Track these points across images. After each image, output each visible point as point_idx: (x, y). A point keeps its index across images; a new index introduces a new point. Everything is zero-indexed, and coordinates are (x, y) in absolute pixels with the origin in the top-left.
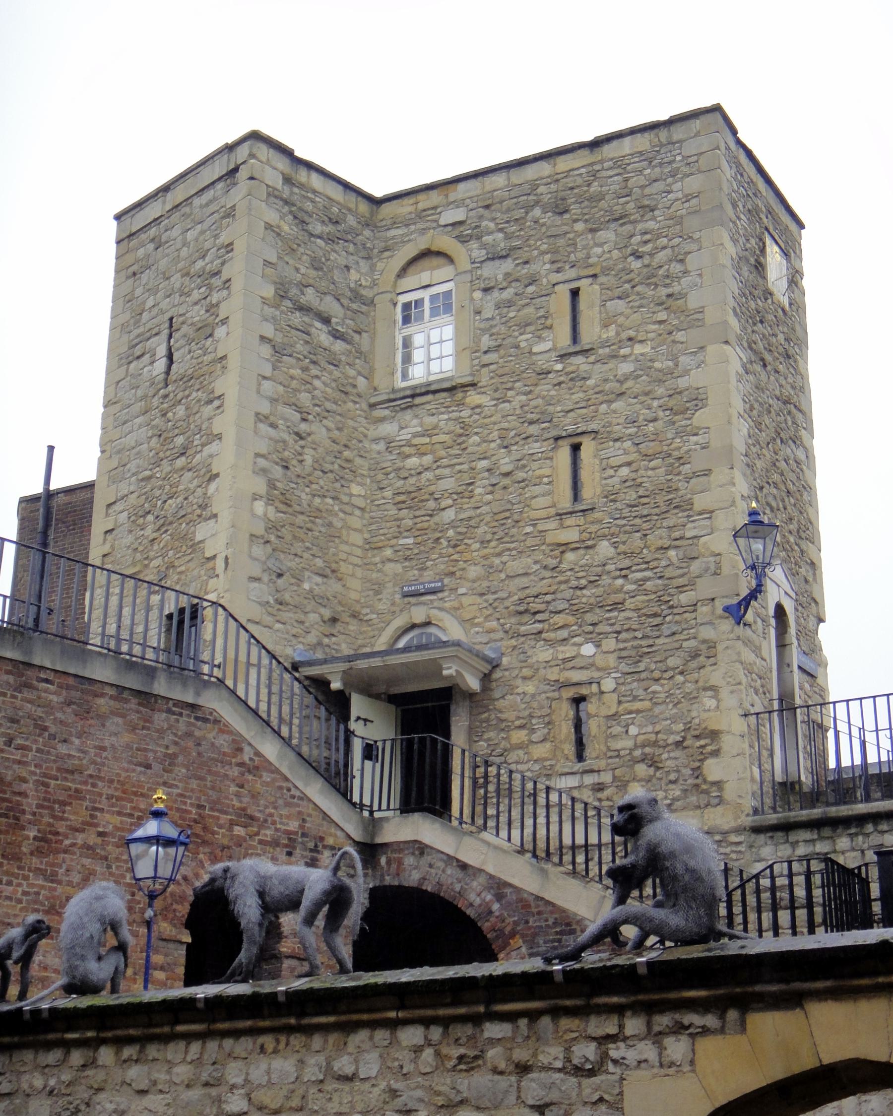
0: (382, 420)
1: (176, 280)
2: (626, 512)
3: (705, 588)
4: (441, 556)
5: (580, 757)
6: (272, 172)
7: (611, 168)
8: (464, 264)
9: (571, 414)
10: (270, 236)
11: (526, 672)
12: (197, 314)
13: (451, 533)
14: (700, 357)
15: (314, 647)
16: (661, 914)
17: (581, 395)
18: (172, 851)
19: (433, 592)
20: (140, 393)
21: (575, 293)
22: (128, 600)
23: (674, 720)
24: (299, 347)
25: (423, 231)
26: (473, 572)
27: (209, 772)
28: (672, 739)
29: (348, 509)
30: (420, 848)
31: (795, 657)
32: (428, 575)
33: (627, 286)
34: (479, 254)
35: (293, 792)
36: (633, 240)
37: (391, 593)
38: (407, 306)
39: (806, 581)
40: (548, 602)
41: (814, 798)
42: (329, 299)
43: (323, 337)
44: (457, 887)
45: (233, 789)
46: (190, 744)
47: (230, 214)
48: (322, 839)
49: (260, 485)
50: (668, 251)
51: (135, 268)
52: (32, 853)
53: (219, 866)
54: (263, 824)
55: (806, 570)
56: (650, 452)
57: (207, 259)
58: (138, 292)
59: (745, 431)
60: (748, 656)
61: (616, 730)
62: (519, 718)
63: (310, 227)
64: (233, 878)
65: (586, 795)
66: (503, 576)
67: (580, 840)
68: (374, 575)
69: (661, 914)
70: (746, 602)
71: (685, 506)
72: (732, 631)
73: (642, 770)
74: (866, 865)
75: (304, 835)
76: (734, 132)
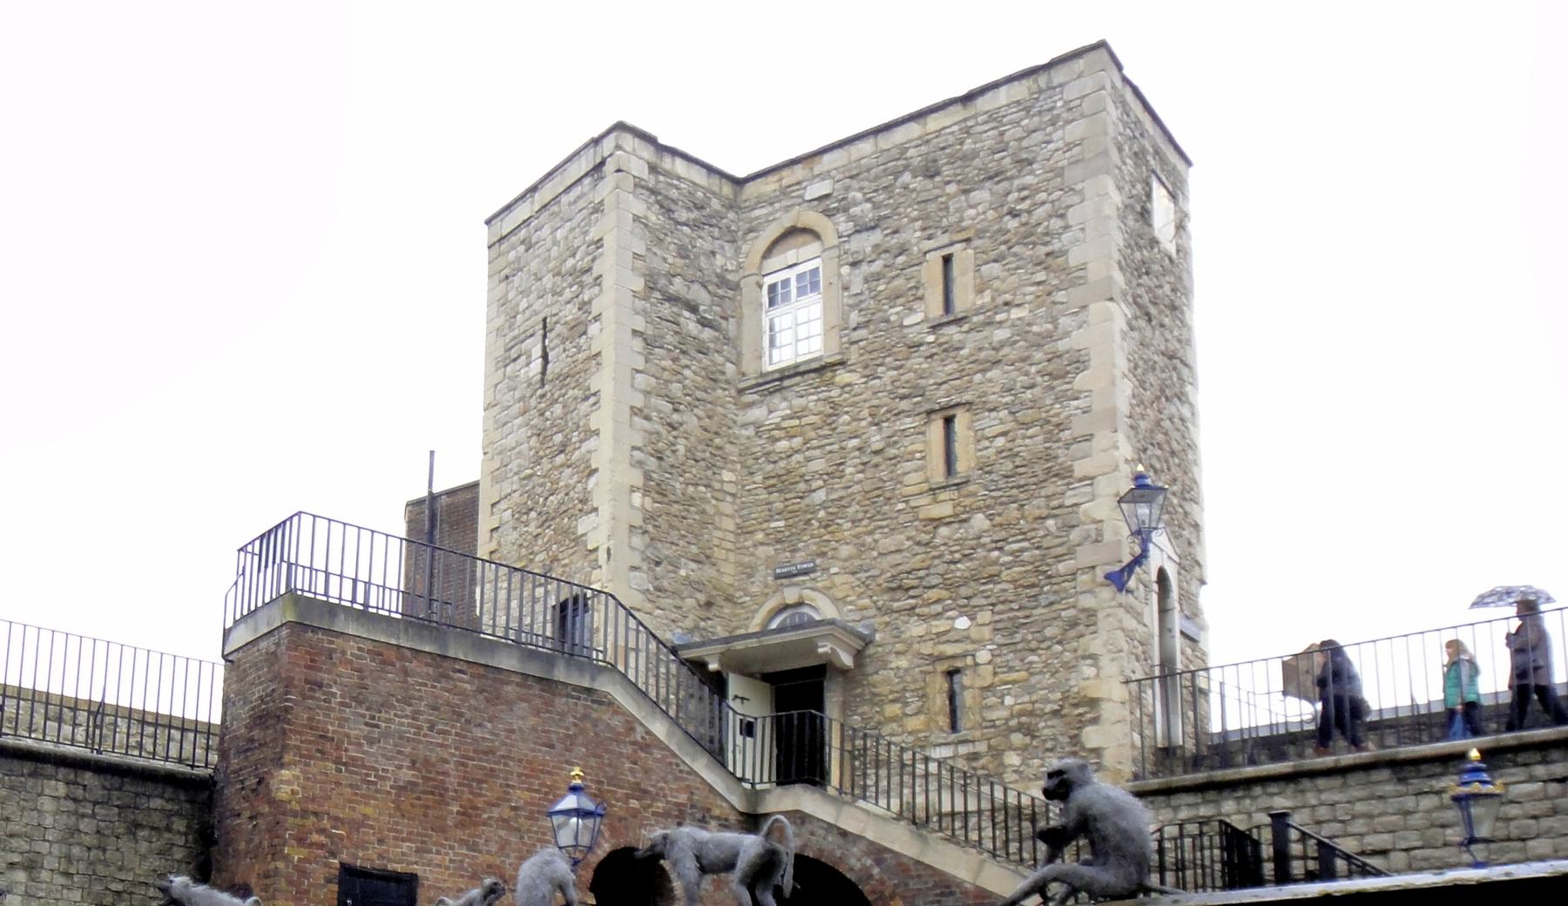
0: (751, 405)
1: (548, 281)
2: (1002, 484)
3: (1085, 556)
4: (813, 537)
5: (954, 727)
6: (637, 161)
7: (985, 122)
8: (831, 239)
9: (945, 386)
10: (639, 228)
11: (899, 647)
12: (570, 313)
13: (822, 514)
14: (1082, 316)
15: (691, 631)
16: (1089, 872)
17: (955, 366)
18: (590, 822)
19: (805, 573)
20: (517, 395)
21: (947, 260)
22: (515, 593)
23: (1051, 688)
24: (669, 338)
25: (787, 209)
26: (845, 551)
27: (607, 751)
28: (1048, 708)
29: (718, 495)
30: (800, 817)
31: (1177, 622)
32: (800, 556)
33: (1003, 247)
34: (846, 227)
35: (682, 767)
36: (1010, 198)
37: (763, 575)
38: (772, 288)
39: (1190, 544)
40: (921, 578)
41: (1196, 762)
42: (696, 287)
43: (692, 327)
44: (838, 853)
45: (628, 765)
46: (588, 725)
47: (598, 209)
48: (709, 810)
49: (637, 478)
50: (1048, 207)
51: (506, 271)
52: (456, 826)
53: (658, 832)
54: (655, 798)
55: (1187, 531)
56: (1028, 420)
57: (578, 257)
58: (511, 295)
59: (1129, 392)
60: (1130, 622)
61: (993, 700)
62: (892, 692)
63: (676, 215)
64: (672, 844)
65: (961, 764)
66: (875, 554)
67: (959, 807)
68: (747, 559)
69: (1089, 872)
70: (1130, 568)
71: (1065, 474)
72: (1114, 599)
73: (1017, 739)
74: (1258, 827)
75: (692, 807)
76: (1119, 67)
